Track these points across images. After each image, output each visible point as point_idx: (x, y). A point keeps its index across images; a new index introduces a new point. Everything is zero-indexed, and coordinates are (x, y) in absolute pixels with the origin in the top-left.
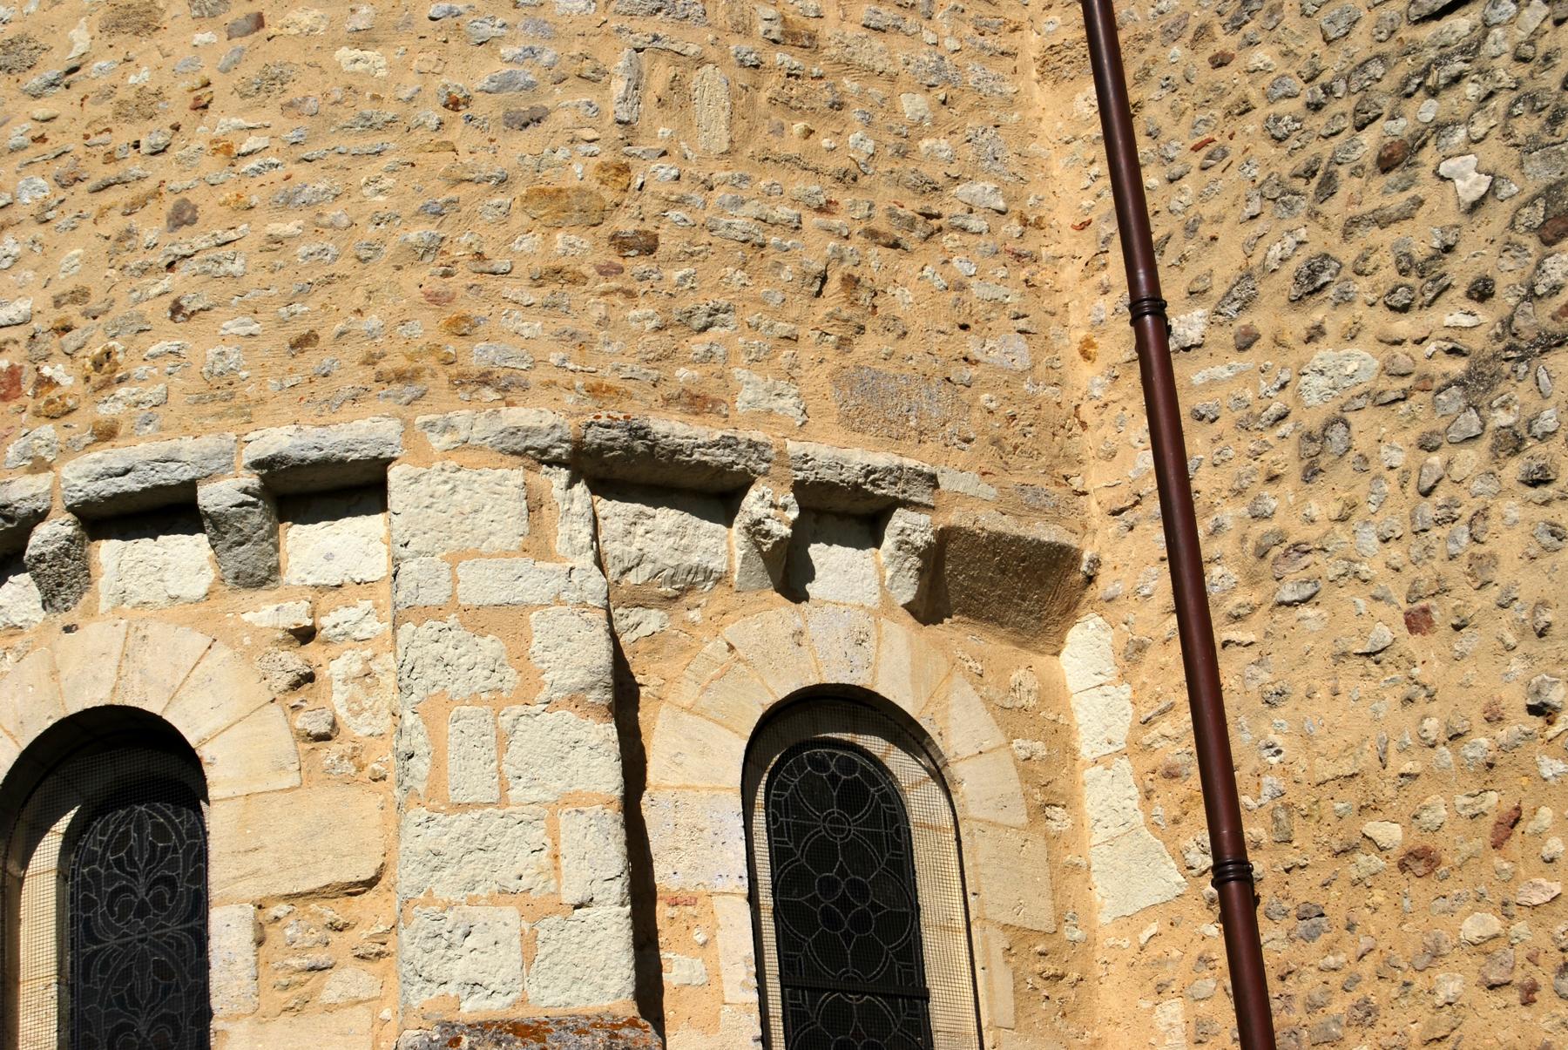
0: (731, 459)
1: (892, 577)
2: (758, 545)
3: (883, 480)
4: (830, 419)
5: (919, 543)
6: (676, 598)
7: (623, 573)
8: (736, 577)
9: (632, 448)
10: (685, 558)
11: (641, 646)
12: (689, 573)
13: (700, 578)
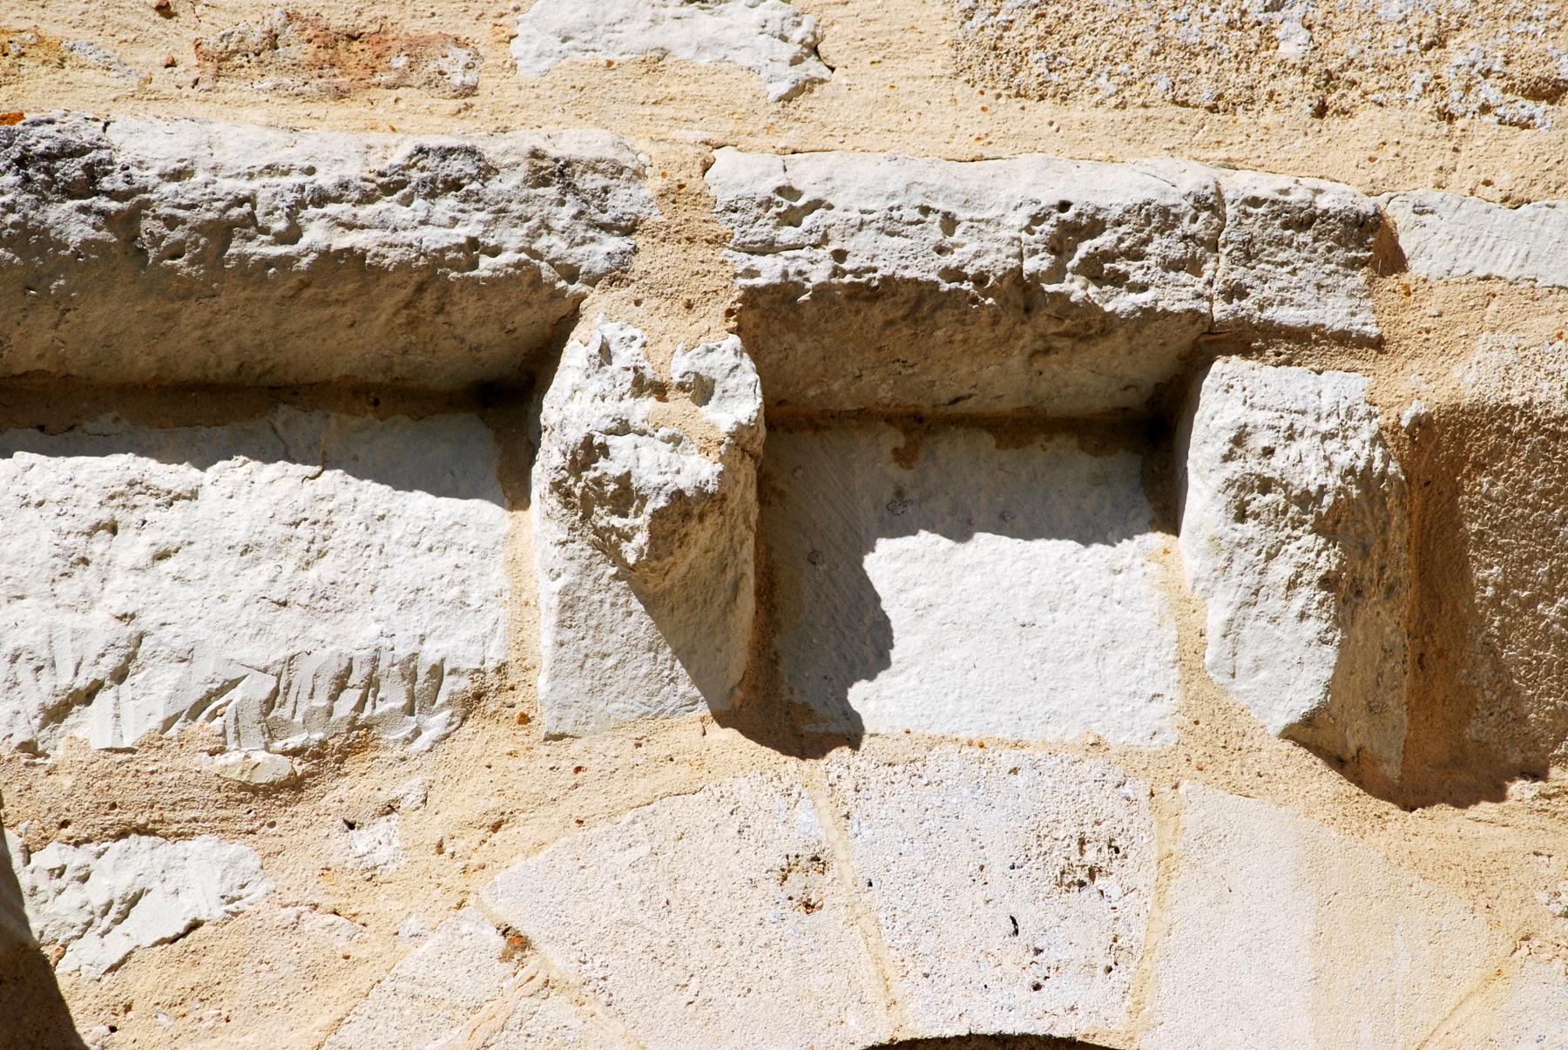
0: (460, 234)
1: (1231, 629)
2: (607, 544)
3: (1135, 255)
4: (918, 66)
5: (1311, 476)
6: (296, 785)
7: (56, 714)
8: (542, 683)
9: (42, 231)
10: (319, 630)
11: (141, 983)
12: (341, 683)
13: (392, 698)
